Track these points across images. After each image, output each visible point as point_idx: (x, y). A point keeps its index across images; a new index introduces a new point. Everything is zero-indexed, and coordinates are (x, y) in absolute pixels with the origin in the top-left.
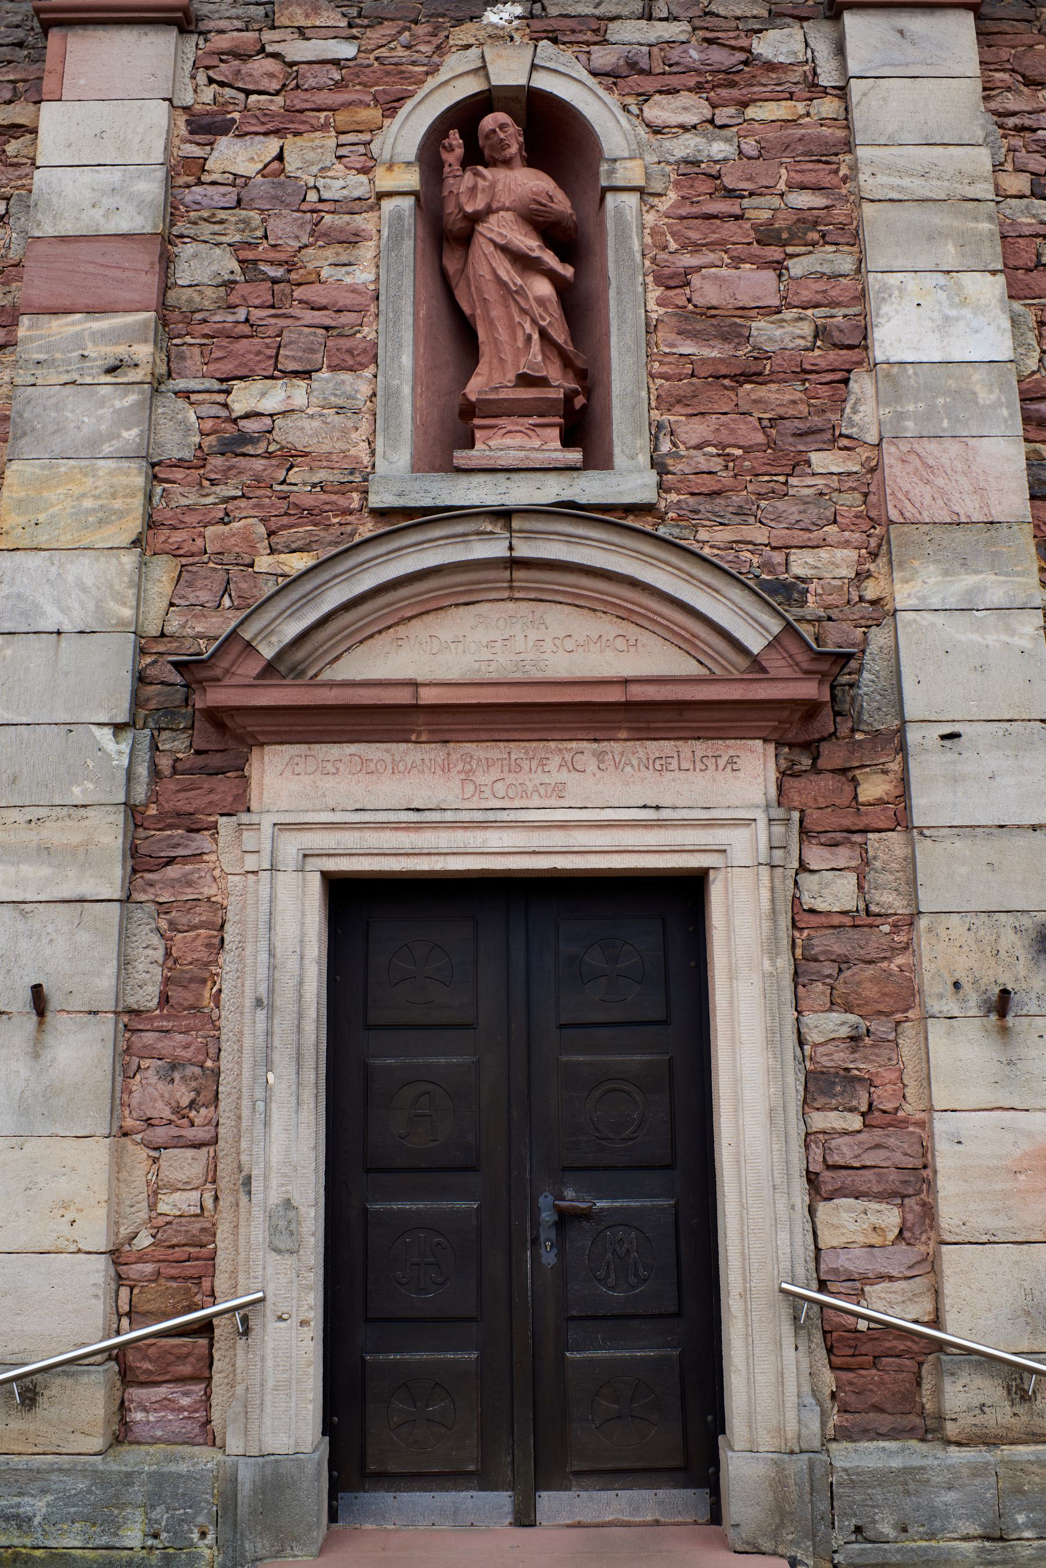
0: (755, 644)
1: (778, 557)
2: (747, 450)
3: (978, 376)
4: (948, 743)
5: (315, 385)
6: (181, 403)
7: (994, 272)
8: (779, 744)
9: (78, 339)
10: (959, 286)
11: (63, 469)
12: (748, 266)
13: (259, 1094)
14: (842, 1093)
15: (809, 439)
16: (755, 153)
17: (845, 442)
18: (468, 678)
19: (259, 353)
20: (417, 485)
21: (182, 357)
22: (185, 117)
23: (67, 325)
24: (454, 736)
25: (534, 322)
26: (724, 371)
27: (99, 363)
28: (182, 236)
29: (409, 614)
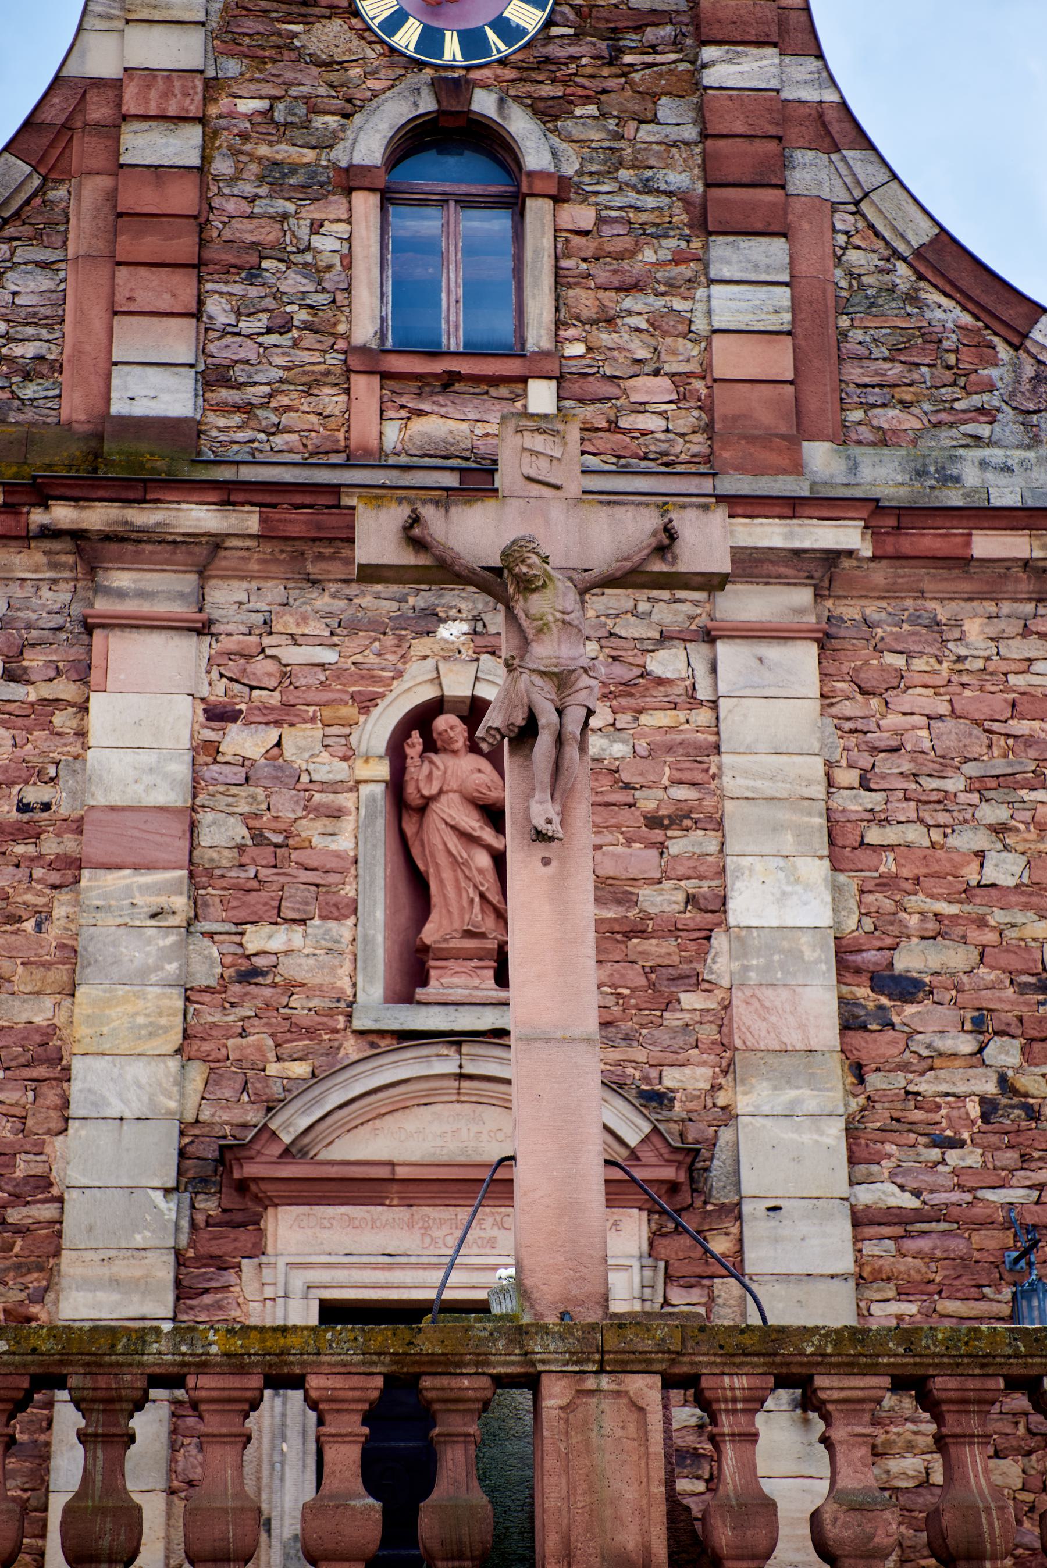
0: (633, 1140)
1: (653, 1073)
2: (633, 990)
3: (805, 939)
4: (772, 1214)
5: (309, 931)
6: (207, 941)
7: (821, 858)
8: (650, 1212)
9: (128, 889)
10: (795, 867)
11: (120, 993)
12: (638, 845)
13: (277, 1458)
14: (691, 1465)
15: (680, 982)
16: (645, 753)
17: (706, 986)
18: (428, 1160)
19: (266, 904)
20: (389, 1014)
21: (206, 905)
22: (203, 706)
23: (119, 878)
24: (417, 1202)
25: (476, 887)
26: (617, 928)
27: (145, 910)
28: (203, 806)
29: (383, 1111)
